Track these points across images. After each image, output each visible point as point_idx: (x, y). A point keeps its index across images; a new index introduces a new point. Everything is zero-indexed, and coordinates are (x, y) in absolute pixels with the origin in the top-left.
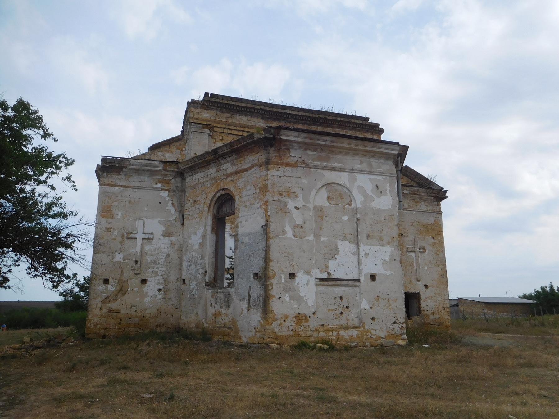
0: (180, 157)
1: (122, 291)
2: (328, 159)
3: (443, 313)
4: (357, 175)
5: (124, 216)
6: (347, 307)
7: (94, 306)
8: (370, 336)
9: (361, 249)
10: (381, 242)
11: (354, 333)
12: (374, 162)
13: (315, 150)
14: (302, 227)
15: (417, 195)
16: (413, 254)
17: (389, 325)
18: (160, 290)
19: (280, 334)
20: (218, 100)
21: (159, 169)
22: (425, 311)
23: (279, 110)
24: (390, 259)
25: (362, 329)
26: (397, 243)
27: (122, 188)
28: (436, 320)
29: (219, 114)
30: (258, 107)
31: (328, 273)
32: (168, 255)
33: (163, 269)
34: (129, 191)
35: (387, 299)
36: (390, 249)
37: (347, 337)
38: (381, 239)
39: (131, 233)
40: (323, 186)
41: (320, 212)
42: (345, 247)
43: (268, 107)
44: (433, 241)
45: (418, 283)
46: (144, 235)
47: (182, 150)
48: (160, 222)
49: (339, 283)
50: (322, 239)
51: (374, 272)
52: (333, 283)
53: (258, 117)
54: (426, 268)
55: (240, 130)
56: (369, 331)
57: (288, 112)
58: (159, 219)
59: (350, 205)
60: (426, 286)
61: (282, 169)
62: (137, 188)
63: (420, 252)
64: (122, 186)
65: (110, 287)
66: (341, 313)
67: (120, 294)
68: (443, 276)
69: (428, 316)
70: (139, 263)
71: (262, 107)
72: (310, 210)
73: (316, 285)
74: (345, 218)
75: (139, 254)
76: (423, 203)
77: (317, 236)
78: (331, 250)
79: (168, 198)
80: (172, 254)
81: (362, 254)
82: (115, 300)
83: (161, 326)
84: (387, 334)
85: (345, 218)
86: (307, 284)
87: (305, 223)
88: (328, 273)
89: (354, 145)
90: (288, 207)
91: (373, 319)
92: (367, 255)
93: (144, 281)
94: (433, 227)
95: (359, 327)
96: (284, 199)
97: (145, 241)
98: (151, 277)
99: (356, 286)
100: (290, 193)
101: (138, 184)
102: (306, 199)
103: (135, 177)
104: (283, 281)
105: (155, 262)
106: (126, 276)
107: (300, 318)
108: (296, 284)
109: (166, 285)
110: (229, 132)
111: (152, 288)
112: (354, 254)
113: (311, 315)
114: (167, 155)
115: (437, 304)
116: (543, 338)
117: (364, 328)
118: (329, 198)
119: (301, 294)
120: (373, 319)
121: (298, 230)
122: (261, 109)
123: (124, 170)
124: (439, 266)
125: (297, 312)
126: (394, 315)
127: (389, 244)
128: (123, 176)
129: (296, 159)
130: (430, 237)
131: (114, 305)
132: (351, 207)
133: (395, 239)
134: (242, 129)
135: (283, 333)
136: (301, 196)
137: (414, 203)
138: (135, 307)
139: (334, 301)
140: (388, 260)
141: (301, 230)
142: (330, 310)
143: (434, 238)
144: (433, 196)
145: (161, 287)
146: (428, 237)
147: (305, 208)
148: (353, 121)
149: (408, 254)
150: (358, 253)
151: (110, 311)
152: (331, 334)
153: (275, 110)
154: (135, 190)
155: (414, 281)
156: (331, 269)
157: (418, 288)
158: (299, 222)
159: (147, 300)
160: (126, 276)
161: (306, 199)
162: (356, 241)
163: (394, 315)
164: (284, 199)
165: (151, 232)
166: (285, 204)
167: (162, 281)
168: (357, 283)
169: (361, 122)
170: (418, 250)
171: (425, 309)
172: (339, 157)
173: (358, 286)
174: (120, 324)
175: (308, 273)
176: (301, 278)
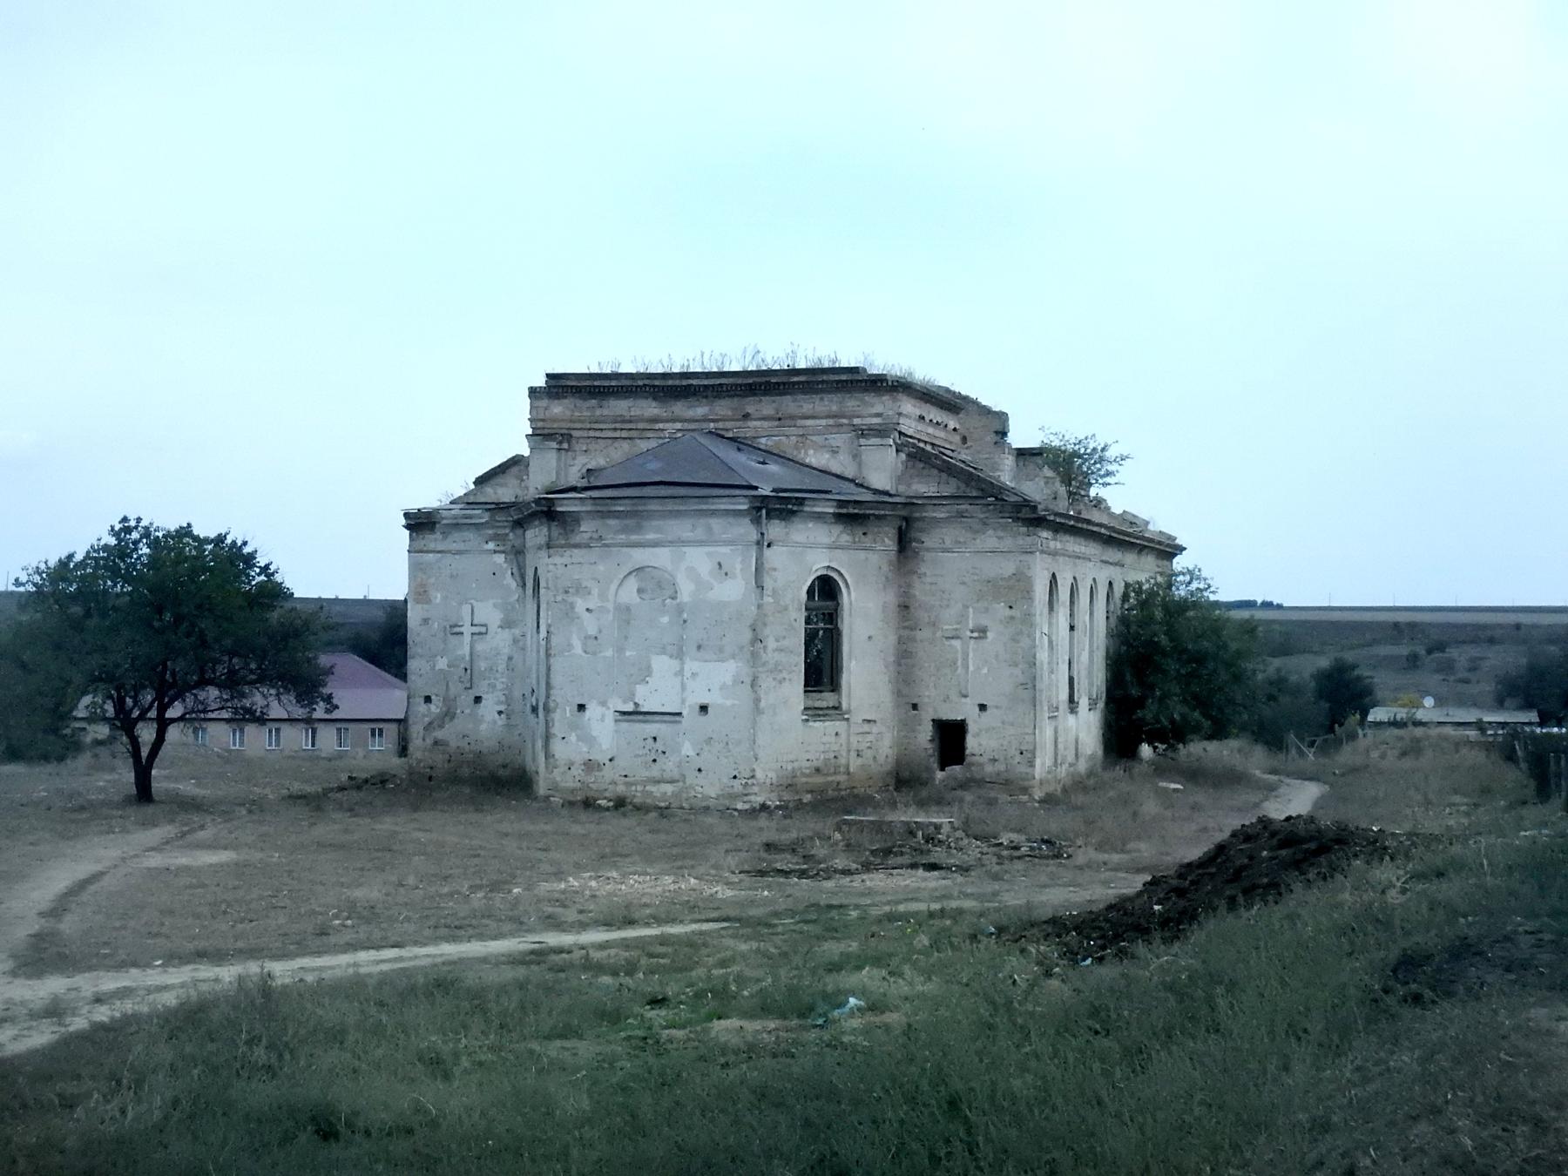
0: (520, 493)
1: (449, 714)
2: (638, 529)
3: (1016, 762)
4: (684, 549)
5: (445, 598)
6: (664, 753)
7: (415, 735)
8: (693, 793)
9: (686, 667)
10: (721, 654)
12: (716, 524)
13: (618, 518)
14: (596, 638)
15: (972, 517)
16: (957, 643)
17: (725, 780)
18: (500, 713)
19: (563, 784)
20: (570, 383)
21: (483, 521)
22: (973, 755)
23: (677, 382)
24: (734, 681)
25: (681, 784)
27: (439, 555)
28: (998, 774)
29: (579, 403)
30: (640, 383)
31: (635, 704)
32: (510, 658)
33: (504, 680)
34: (449, 558)
35: (725, 742)
36: (735, 665)
38: (721, 650)
39: (456, 626)
40: (630, 573)
41: (625, 611)
42: (662, 665)
43: (672, 378)
44: (1008, 612)
45: (963, 700)
46: (474, 628)
47: (522, 480)
48: (495, 606)
49: (649, 717)
50: (628, 654)
51: (704, 701)
52: (641, 717)
53: (647, 398)
54: (985, 671)
55: (615, 429)
56: (692, 787)
57: (695, 382)
58: (495, 601)
59: (673, 598)
60: (983, 707)
61: (568, 553)
62: (459, 552)
63: (971, 638)
64: (439, 552)
65: (433, 707)
66: (655, 761)
67: (447, 719)
69: (981, 765)
70: (469, 671)
71: (647, 382)
72: (608, 611)
73: (616, 721)
74: (665, 620)
75: (468, 658)
76: (991, 532)
77: (620, 650)
78: (640, 669)
79: (505, 565)
80: (516, 656)
81: (687, 674)
82: (441, 726)
83: (504, 766)
84: (720, 793)
85: (665, 620)
86: (603, 720)
87: (600, 632)
88: (635, 704)
89: (671, 506)
90: (576, 610)
91: (700, 770)
92: (694, 675)
93: (478, 699)
95: (678, 781)
96: (570, 599)
97: (475, 637)
98: (487, 693)
99: (676, 722)
100: (581, 590)
101: (461, 546)
102: (603, 596)
103: (456, 535)
104: (568, 715)
105: (491, 669)
106: (453, 691)
107: (590, 766)
108: (587, 718)
109: (509, 705)
110: (598, 434)
111: (489, 708)
112: (676, 674)
113: (607, 762)
114: (500, 491)
115: (1005, 743)
117: (684, 783)
118: (640, 591)
119: (594, 734)
120: (700, 770)
121: (591, 642)
122: (645, 385)
123: (437, 526)
124: (1017, 666)
125: (587, 757)
127: (734, 658)
128: (438, 535)
129: (589, 535)
131: (439, 734)
132: (674, 602)
133: (745, 649)
134: (618, 426)
135: (568, 785)
136: (595, 591)
137: (969, 535)
138: (624, 713)
139: (642, 743)
141: (595, 642)
142: (637, 756)
143: (1011, 607)
145: (502, 708)
146: (997, 606)
147: (602, 609)
148: (825, 378)
149: (947, 643)
150: (680, 673)
151: (436, 743)
152: (633, 788)
153: (670, 382)
154: (457, 557)
155: (954, 697)
158: (592, 631)
159: (483, 727)
160: (453, 691)
161: (603, 596)
162: (679, 655)
163: (735, 766)
164: (570, 599)
165: (483, 622)
166: (572, 606)
167: (503, 698)
168: (677, 718)
169: (844, 377)
170: (969, 634)
171: (977, 751)
172: (655, 523)
174: (449, 761)
175: (603, 704)
176: (593, 711)
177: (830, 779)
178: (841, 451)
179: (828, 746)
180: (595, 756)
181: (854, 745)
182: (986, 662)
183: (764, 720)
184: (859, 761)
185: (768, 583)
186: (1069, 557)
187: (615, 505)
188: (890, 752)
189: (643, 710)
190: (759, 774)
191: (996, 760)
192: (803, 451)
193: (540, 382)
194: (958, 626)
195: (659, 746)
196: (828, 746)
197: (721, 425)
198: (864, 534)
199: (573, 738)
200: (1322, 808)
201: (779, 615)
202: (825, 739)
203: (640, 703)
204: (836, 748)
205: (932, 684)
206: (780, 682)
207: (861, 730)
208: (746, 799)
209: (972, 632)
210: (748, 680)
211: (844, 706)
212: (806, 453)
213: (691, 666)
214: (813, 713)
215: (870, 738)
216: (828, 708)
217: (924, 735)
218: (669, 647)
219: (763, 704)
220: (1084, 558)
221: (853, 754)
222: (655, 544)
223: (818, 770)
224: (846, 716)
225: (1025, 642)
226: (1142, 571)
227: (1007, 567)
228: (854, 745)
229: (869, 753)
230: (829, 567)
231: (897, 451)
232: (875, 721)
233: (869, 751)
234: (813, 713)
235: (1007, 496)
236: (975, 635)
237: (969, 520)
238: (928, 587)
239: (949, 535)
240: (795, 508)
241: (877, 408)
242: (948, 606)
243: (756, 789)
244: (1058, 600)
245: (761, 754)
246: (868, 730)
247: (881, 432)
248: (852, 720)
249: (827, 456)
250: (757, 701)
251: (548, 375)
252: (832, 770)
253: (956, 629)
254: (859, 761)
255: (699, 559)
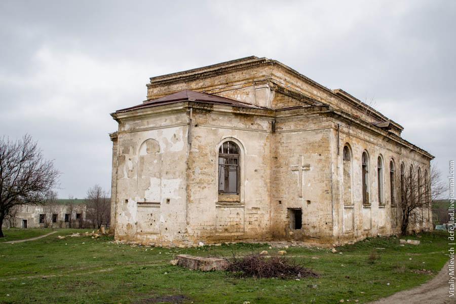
4: (162, 130)
7: (112, 216)
11: (155, 237)
15: (302, 115)
16: (297, 173)
22: (305, 224)
23: (191, 74)
24: (179, 188)
25: (160, 235)
26: (185, 176)
37: (151, 240)
42: (154, 181)
43: (189, 73)
45: (300, 199)
49: (149, 205)
51: (169, 197)
52: (146, 205)
54: (309, 185)
60: (309, 202)
66: (151, 224)
68: (327, 192)
74: (155, 161)
84: (174, 240)
87: (133, 168)
94: (320, 144)
95: (158, 234)
115: (319, 219)
116: (371, 261)
126: (179, 227)
130: (316, 154)
138: (140, 203)
140: (178, 189)
142: (146, 222)
144: (318, 113)
148: (242, 63)
149: (293, 173)
153: (188, 75)
155: (297, 198)
156: (146, 197)
157: (301, 204)
162: (160, 177)
168: (158, 205)
170: (302, 168)
173: (159, 207)
175: (133, 199)
177: (233, 234)
178: (250, 94)
179: (232, 219)
180: (131, 223)
181: (248, 219)
182: (310, 181)
183: (192, 206)
184: (250, 227)
185: (195, 142)
186: (361, 140)
187: (137, 113)
188: (268, 223)
189: (148, 202)
190: (190, 231)
191: (315, 227)
192: (236, 96)
193: (149, 82)
194: (298, 165)
195: (153, 218)
196: (232, 219)
197: (207, 89)
198: (252, 124)
199: (123, 214)
200: (410, 248)
201: (203, 158)
202: (231, 216)
203: (146, 198)
204: (238, 220)
205: (287, 192)
206: (203, 188)
207: (251, 212)
208: (183, 242)
209: (303, 167)
210: (185, 187)
211: (242, 201)
212: (237, 97)
213: (164, 181)
214: (221, 204)
215: (256, 216)
216: (234, 202)
217: (284, 217)
218: (156, 174)
219: (192, 198)
220: (411, 171)
221: (247, 223)
222: (152, 129)
223: (226, 230)
224: (242, 206)
225: (327, 171)
226: (411, 161)
227: (319, 137)
228: (248, 219)
229: (257, 223)
230: (231, 137)
231: (271, 90)
232: (259, 209)
233: (256, 222)
234: (221, 204)
235: (316, 103)
236: (305, 168)
237: (301, 116)
238: (284, 148)
239: (291, 125)
240: (209, 109)
241: (264, 72)
242: (293, 156)
243: (188, 238)
244: (352, 155)
245: (191, 222)
246: (256, 212)
247: (263, 82)
248: (246, 207)
249: (245, 96)
250: (188, 196)
251: (151, 79)
252: (235, 230)
253: (297, 167)
254: (250, 227)
255: (169, 133)
